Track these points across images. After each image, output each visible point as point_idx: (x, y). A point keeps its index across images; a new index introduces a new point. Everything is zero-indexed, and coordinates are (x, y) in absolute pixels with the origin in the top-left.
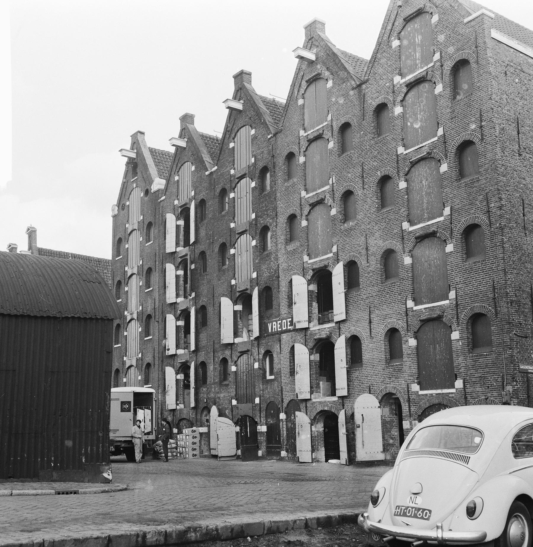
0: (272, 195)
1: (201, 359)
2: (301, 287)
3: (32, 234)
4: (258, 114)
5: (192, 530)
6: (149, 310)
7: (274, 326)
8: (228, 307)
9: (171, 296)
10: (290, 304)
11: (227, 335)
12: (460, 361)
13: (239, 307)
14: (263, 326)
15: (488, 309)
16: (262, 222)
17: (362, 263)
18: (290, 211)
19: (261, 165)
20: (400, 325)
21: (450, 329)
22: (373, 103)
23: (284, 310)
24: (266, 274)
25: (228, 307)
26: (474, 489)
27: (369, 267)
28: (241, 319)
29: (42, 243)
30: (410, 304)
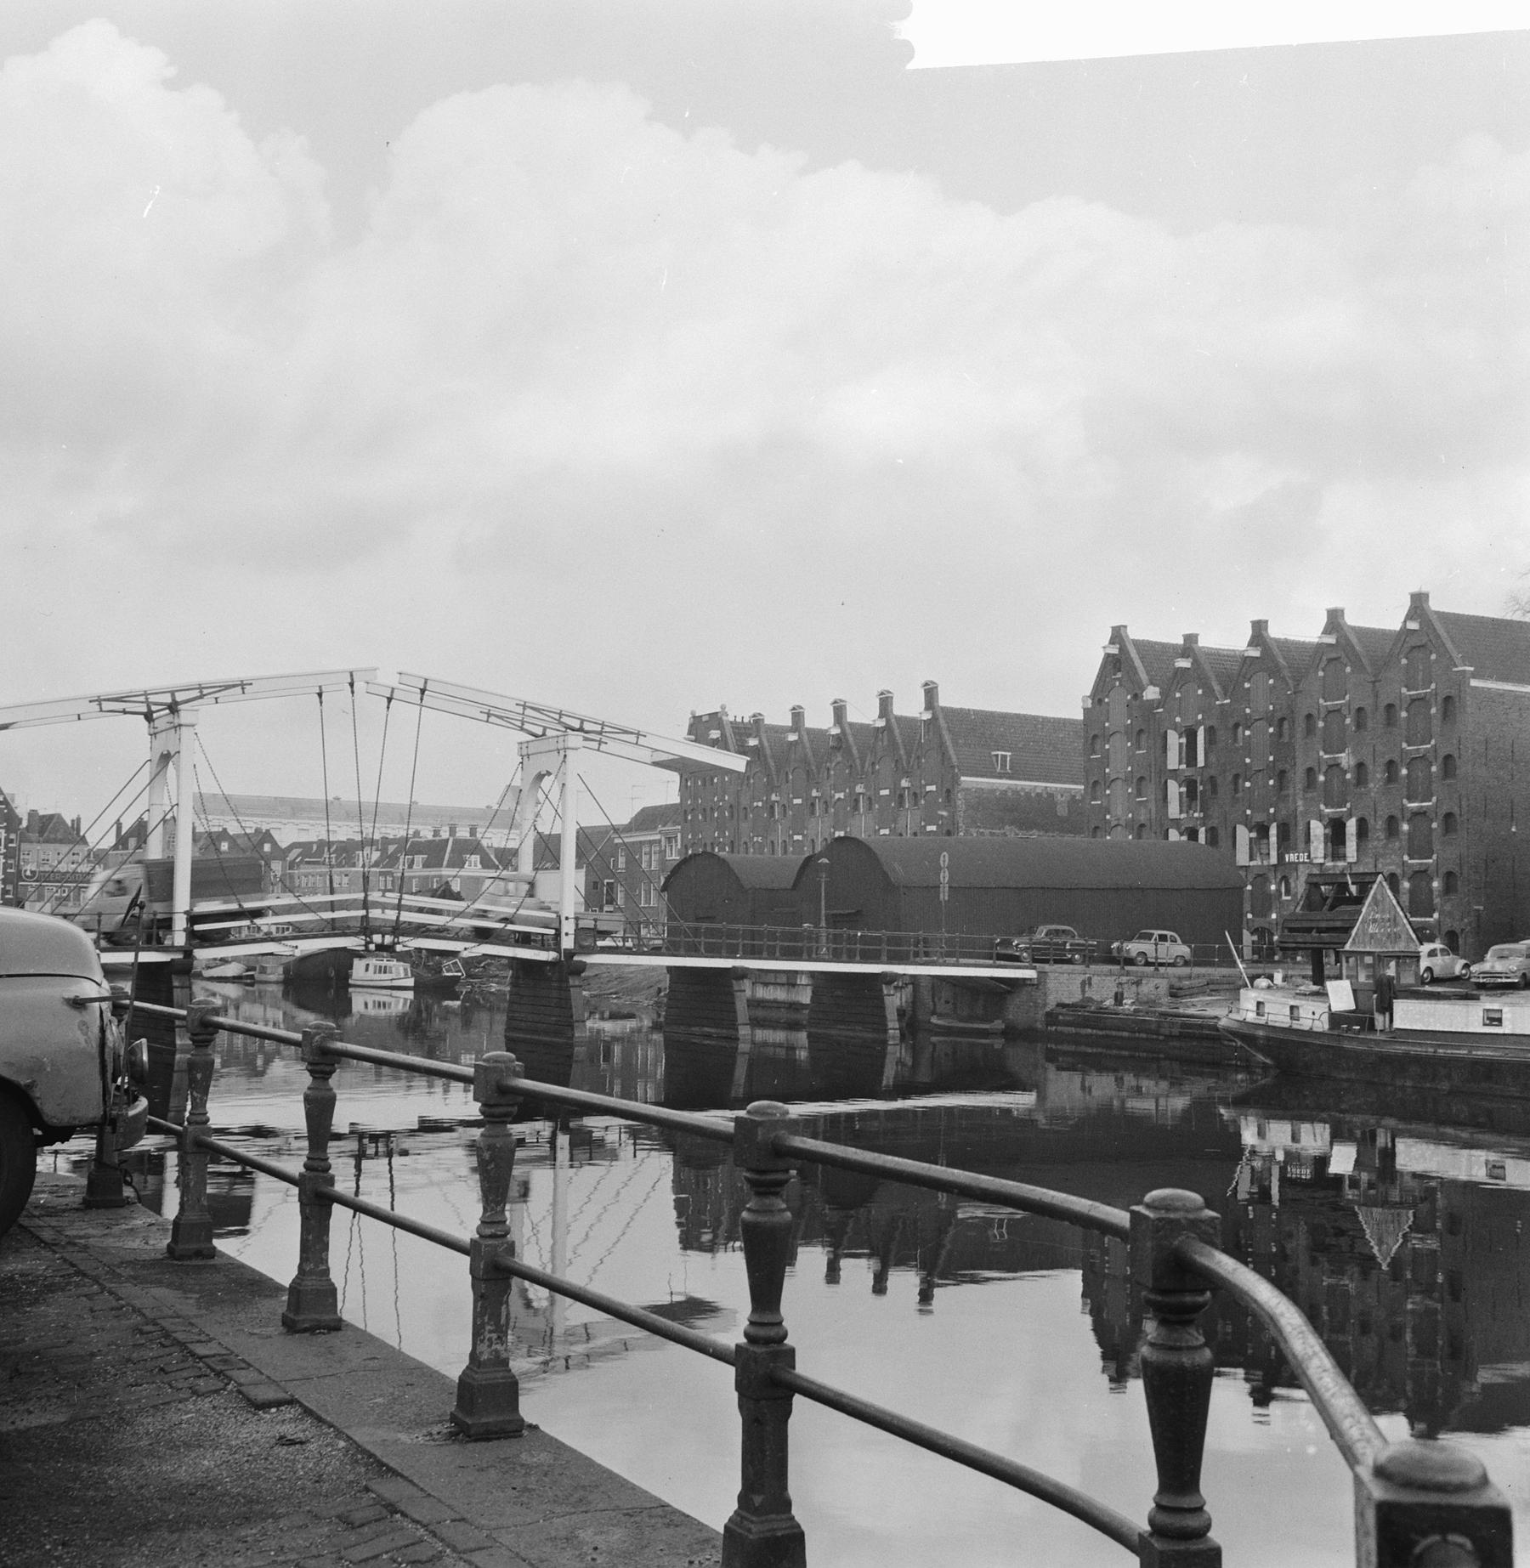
0: (1290, 746)
1: (1210, 824)
2: (1318, 829)
3: (931, 692)
4: (1273, 659)
5: (1358, 1133)
6: (1142, 819)
7: (1291, 857)
8: (1243, 835)
9: (1174, 810)
10: (1308, 841)
11: (1242, 858)
12: (1437, 901)
13: (1254, 835)
14: (1281, 857)
15: (1456, 870)
16: (1280, 766)
17: (1371, 822)
18: (1308, 765)
19: (1279, 715)
20: (1399, 871)
21: (1432, 879)
22: (1384, 702)
23: (1301, 845)
24: (1284, 812)
25: (1243, 835)
26: (355, 1249)
27: (1378, 826)
28: (1256, 847)
29: (945, 700)
30: (1406, 858)
